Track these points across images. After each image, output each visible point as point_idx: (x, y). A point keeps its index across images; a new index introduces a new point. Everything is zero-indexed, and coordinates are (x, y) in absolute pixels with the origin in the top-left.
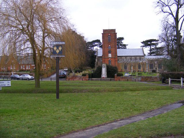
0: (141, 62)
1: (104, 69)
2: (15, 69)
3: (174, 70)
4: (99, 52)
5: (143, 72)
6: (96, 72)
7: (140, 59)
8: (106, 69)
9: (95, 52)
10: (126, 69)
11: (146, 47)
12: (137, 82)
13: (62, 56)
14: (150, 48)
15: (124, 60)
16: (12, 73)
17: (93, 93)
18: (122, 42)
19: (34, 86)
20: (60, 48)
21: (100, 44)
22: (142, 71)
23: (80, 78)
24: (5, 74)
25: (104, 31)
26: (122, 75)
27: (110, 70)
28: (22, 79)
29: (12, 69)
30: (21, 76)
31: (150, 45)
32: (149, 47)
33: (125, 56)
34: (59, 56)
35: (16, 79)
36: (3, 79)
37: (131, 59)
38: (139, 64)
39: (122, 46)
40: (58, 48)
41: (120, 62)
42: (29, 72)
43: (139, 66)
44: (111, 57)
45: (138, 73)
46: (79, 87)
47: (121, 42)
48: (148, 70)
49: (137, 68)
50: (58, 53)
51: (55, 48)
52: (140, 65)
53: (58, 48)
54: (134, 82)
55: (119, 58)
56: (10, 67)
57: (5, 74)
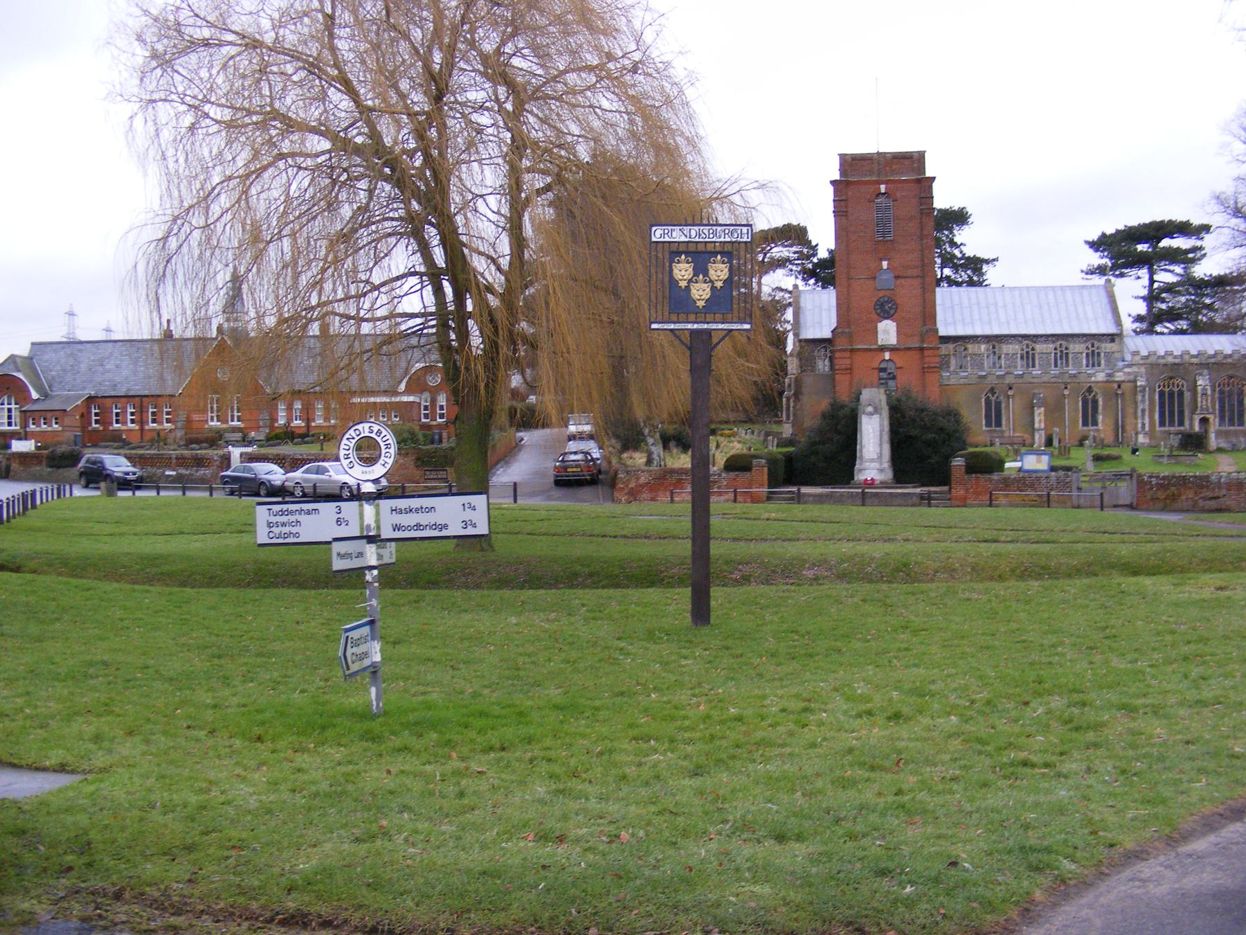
0: (1101, 377)
3: (1104, 446)
5: (1118, 443)
6: (814, 444)
7: (1093, 358)
8: (886, 423)
9: (775, 308)
10: (999, 424)
11: (1122, 275)
12: (1109, 514)
13: (735, 326)
14: (1146, 281)
15: (981, 368)
16: (236, 452)
17: (1093, 580)
18: (958, 240)
20: (719, 271)
22: (1109, 439)
24: (181, 461)
25: (850, 163)
26: (998, 465)
27: (914, 432)
29: (215, 424)
30: (298, 475)
32: (1144, 273)
33: (988, 339)
34: (714, 326)
35: (263, 492)
37: (1029, 358)
38: (1090, 390)
39: (956, 268)
40: (701, 269)
41: (952, 381)
43: (1085, 402)
46: (779, 548)
47: (953, 244)
48: (1151, 434)
50: (701, 304)
51: (683, 271)
52: (1095, 402)
53: (701, 269)
54: (1087, 513)
56: (205, 411)
57: (181, 461)
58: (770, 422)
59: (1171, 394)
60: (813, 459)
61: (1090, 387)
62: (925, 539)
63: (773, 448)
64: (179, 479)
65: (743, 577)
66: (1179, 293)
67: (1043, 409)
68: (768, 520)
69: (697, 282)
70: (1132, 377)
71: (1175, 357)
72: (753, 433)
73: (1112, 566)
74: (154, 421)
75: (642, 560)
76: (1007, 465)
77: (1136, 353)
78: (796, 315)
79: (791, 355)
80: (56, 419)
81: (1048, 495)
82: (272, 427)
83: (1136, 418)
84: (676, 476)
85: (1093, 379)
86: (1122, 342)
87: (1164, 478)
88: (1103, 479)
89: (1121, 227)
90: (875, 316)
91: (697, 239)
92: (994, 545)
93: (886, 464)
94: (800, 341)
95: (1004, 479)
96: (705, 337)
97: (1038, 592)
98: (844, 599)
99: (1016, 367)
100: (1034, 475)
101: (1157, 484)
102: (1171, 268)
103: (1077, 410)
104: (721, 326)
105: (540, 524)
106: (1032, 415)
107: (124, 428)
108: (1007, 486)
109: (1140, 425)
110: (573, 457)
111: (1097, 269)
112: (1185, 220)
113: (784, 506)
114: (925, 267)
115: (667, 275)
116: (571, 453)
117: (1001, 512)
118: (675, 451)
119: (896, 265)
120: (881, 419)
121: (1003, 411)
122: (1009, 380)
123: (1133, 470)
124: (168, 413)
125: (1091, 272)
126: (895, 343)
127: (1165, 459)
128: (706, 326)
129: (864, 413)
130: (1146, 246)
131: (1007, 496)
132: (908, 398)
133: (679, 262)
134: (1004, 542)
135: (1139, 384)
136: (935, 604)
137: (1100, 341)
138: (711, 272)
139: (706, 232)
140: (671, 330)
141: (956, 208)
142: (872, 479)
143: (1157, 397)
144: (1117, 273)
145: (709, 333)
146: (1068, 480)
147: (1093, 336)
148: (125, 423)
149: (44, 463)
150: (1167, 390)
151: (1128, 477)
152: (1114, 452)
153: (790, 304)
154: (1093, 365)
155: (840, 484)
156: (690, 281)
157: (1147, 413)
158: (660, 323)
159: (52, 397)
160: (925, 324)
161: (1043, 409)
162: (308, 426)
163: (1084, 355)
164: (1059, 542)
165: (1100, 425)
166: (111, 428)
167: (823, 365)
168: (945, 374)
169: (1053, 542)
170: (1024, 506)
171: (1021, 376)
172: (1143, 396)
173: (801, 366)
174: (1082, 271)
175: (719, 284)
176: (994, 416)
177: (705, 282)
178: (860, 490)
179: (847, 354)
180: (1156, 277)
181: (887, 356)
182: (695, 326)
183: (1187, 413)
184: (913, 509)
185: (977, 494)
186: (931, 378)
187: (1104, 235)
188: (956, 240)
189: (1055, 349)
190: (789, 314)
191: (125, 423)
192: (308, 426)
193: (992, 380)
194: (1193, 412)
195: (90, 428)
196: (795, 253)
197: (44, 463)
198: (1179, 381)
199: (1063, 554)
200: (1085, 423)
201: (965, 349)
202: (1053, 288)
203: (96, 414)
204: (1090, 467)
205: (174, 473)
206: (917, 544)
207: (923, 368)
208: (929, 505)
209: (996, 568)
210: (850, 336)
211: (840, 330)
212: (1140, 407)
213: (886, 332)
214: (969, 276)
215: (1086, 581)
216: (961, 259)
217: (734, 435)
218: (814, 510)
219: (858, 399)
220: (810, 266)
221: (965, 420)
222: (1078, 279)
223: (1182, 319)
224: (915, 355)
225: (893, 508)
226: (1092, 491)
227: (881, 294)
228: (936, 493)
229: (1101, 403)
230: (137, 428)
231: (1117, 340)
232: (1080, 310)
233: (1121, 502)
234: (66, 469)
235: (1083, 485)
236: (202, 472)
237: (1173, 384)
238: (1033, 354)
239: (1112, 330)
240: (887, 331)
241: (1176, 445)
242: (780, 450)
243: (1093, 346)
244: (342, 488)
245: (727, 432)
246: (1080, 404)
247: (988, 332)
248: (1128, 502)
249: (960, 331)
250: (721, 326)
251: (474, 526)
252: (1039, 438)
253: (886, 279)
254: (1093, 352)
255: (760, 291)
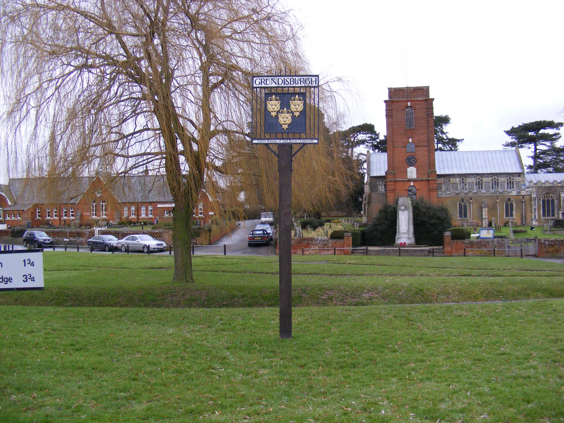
0: (514, 193)
1: (407, 217)
2: (105, 220)
4: (375, 161)
5: (523, 225)
6: (375, 225)
7: (511, 184)
8: (411, 214)
11: (522, 147)
12: (525, 259)
14: (533, 149)
15: (457, 189)
16: (97, 229)
18: (445, 130)
19: (168, 276)
21: (374, 139)
22: (519, 223)
23: (324, 246)
24: (72, 234)
25: (393, 92)
26: (468, 235)
28: (127, 250)
30: (123, 241)
31: (533, 140)
32: (532, 146)
34: (293, 141)
36: (66, 248)
37: (480, 185)
38: (509, 199)
39: (444, 144)
40: (285, 105)
41: (443, 196)
42: (148, 228)
43: (507, 205)
44: (414, 176)
45: (514, 229)
47: (443, 133)
48: (539, 220)
49: (502, 215)
50: (285, 127)
51: (273, 106)
52: (512, 205)
53: (285, 105)
54: (512, 259)
55: (440, 180)
57: (72, 234)
58: (357, 217)
59: (548, 201)
60: (375, 233)
61: (509, 198)
62: (431, 274)
63: (357, 228)
64: (70, 243)
65: (329, 298)
66: (549, 155)
67: (487, 209)
68: (349, 264)
69: (282, 113)
70: (529, 193)
71: (550, 183)
72: (348, 221)
73: (537, 290)
74: (66, 216)
75: (273, 288)
76: (472, 235)
77: (531, 182)
78: (369, 165)
79: (366, 184)
80: (9, 214)
81: (494, 249)
82: (121, 219)
83: (532, 213)
84: (306, 242)
85: (511, 194)
86: (524, 177)
87: (552, 241)
88: (521, 242)
89: (521, 124)
90: (406, 165)
91: (283, 85)
92: (469, 278)
93: (411, 235)
94: (371, 177)
95: (471, 242)
96: (287, 148)
97: (503, 310)
98: (383, 316)
99: (473, 189)
100: (486, 240)
101: (548, 244)
102: (545, 143)
103: (504, 209)
104: (298, 141)
105: (230, 266)
106: (482, 211)
107: (52, 219)
108: (472, 246)
109: (533, 216)
110: (257, 232)
111: (510, 144)
112: (551, 120)
113: (360, 256)
114: (430, 143)
115: (263, 107)
116: (257, 230)
117: (471, 259)
118: (309, 229)
119: (416, 140)
120: (409, 213)
121: (468, 210)
122: (470, 195)
123: (536, 237)
124: (72, 212)
125: (507, 145)
126: (416, 177)
127: (548, 232)
128: (288, 141)
129: (400, 210)
130: (533, 133)
131: (472, 251)
132: (422, 202)
133: (271, 100)
134: (474, 276)
135: (533, 196)
136: (439, 319)
137: (513, 176)
138: (292, 106)
139: (289, 81)
140: (266, 144)
141: (444, 116)
142: (404, 243)
143: (541, 203)
144: (519, 145)
145: (291, 146)
146: (503, 242)
147: (477, 174)
148: (52, 217)
149: (9, 235)
150: (546, 199)
151: (533, 241)
152: (523, 229)
153: (365, 161)
154: (510, 188)
155: (372, 246)
156: (278, 112)
157: (537, 210)
158: (258, 139)
159: (18, 204)
160: (430, 168)
161: (487, 209)
162: (138, 218)
163: (506, 183)
164: (504, 276)
165: (514, 216)
166: (46, 219)
167: (381, 189)
168: (440, 192)
169: (501, 276)
170: (481, 256)
171: (476, 193)
172: (535, 202)
173: (371, 189)
174: (503, 145)
175: (297, 114)
176: (463, 212)
177: (288, 113)
178: (398, 248)
179: (393, 183)
180: (538, 147)
181: (412, 184)
182: (282, 141)
183: (556, 211)
184: (425, 258)
185: (457, 250)
186: (433, 194)
187: (513, 128)
188: (444, 130)
189: (492, 180)
190: (365, 165)
191: (52, 217)
192: (138, 218)
193: (462, 195)
194: (559, 210)
195: (36, 219)
196: (368, 137)
197: (9, 235)
198: (552, 195)
199: (509, 284)
200: (507, 216)
201: (449, 181)
202: (491, 151)
203: (39, 212)
204: (512, 236)
205: (68, 240)
206: (427, 277)
207: (429, 189)
208: (433, 256)
209: (473, 292)
210: (394, 175)
211: (389, 172)
212: (533, 207)
213: (411, 172)
214: (450, 148)
215: (531, 301)
216: (446, 140)
217: (339, 222)
218: (374, 259)
219: (397, 203)
220: (376, 143)
221: (450, 214)
222: (501, 148)
223: (550, 167)
224: (426, 183)
225: (415, 257)
226: (515, 248)
227: (409, 154)
228: (436, 249)
229: (514, 205)
230: (58, 219)
231: (522, 175)
232: (504, 162)
233: (530, 254)
234: (19, 238)
235: (510, 245)
236: (81, 239)
237: (549, 196)
238: (482, 183)
239: (519, 171)
240: (412, 172)
241: (552, 225)
242: (360, 229)
243: (510, 178)
244: (144, 247)
245: (336, 221)
246: (505, 206)
247: (460, 172)
248: (534, 254)
249: (447, 172)
250: (298, 141)
251: (33, 279)
252: (485, 223)
253: (411, 148)
254: (510, 181)
255: (352, 156)
